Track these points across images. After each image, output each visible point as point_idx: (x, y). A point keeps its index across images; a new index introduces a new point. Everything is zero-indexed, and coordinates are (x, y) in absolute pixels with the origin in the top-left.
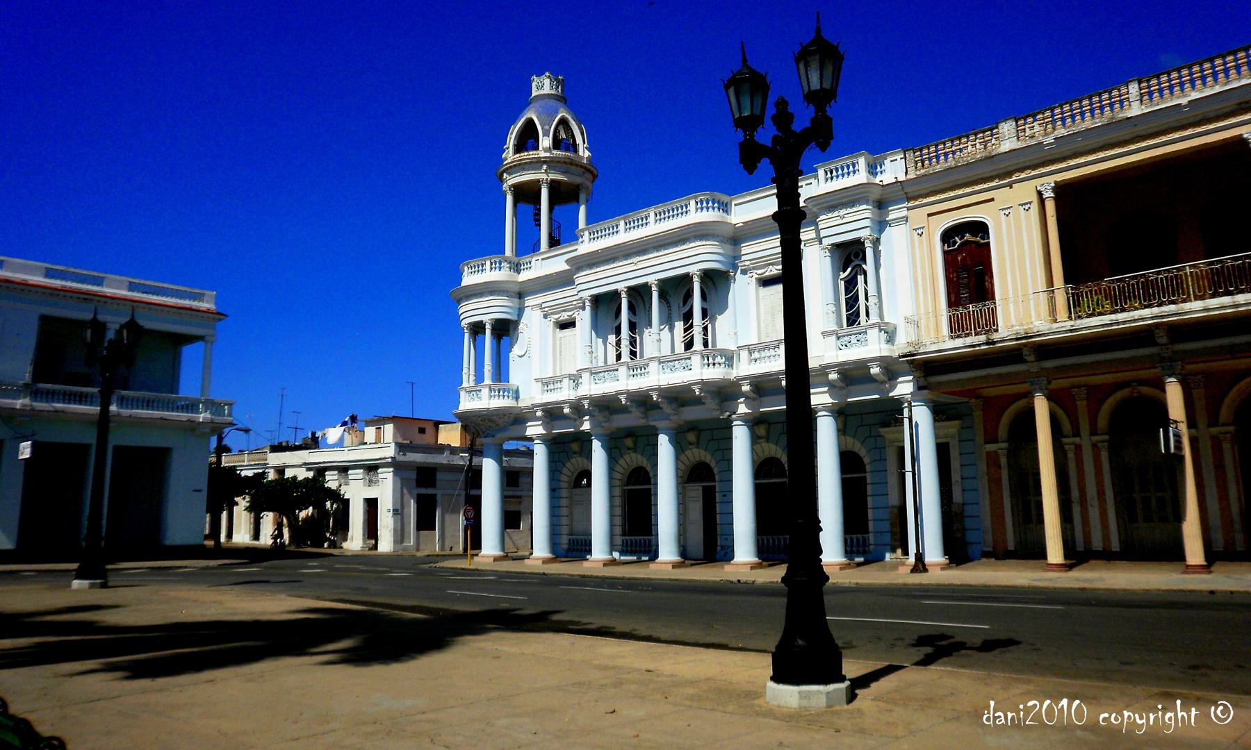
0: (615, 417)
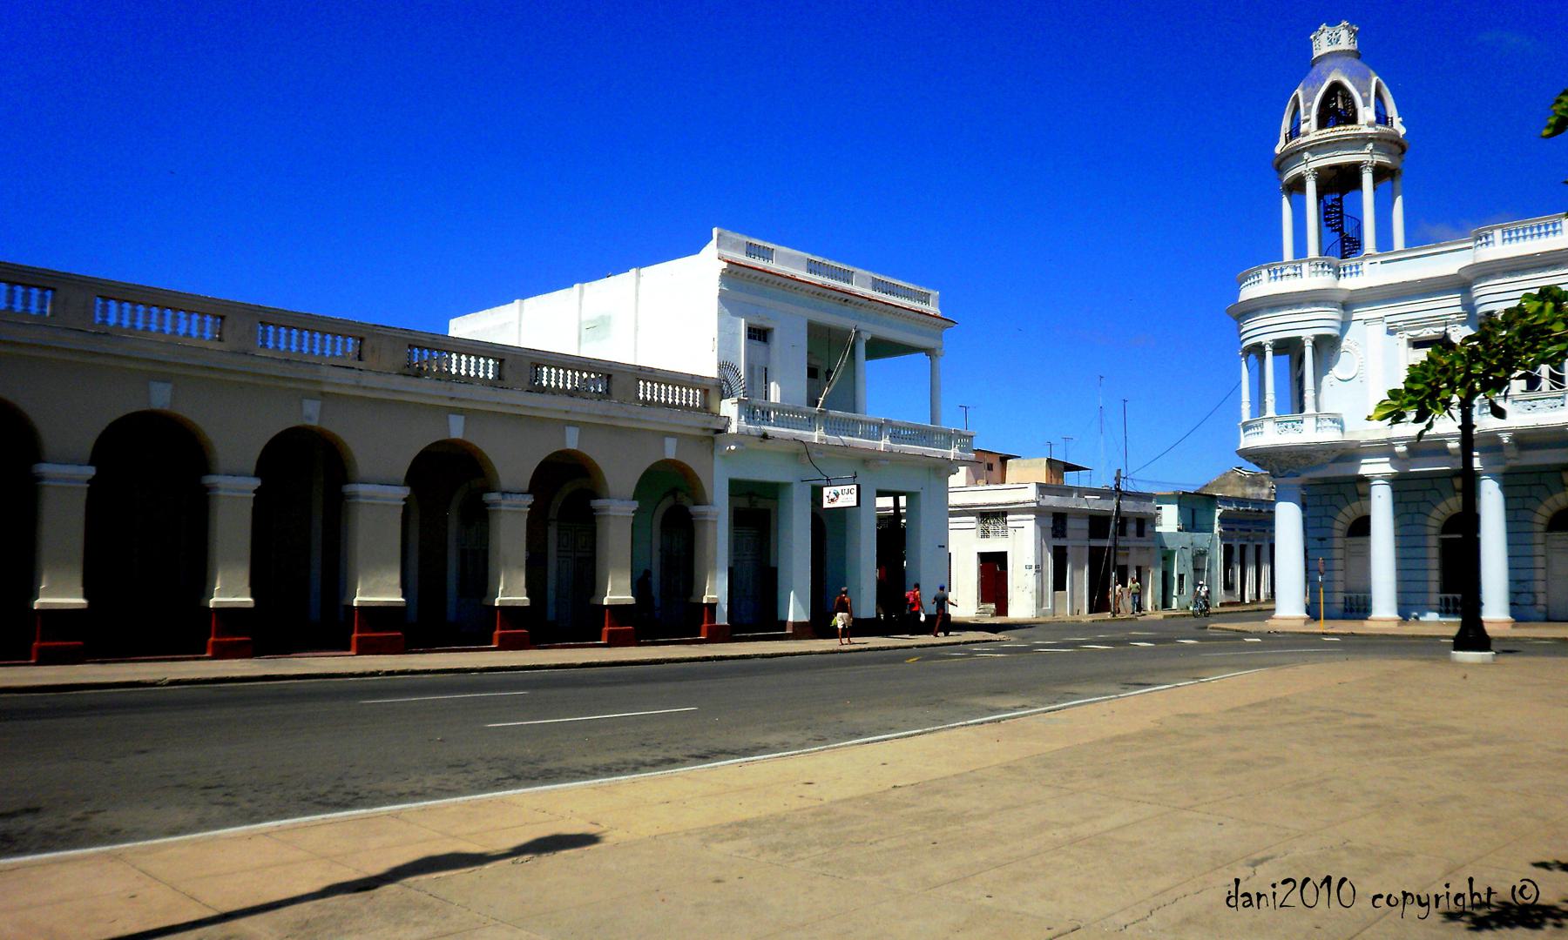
0: (1527, 453)
